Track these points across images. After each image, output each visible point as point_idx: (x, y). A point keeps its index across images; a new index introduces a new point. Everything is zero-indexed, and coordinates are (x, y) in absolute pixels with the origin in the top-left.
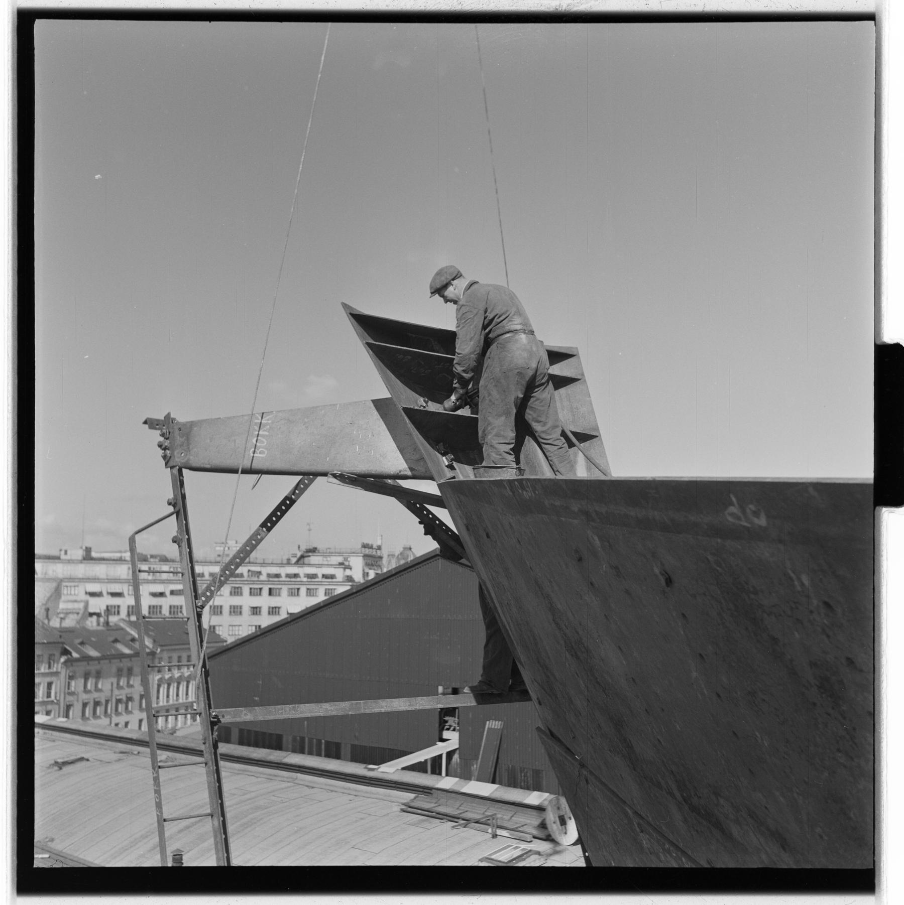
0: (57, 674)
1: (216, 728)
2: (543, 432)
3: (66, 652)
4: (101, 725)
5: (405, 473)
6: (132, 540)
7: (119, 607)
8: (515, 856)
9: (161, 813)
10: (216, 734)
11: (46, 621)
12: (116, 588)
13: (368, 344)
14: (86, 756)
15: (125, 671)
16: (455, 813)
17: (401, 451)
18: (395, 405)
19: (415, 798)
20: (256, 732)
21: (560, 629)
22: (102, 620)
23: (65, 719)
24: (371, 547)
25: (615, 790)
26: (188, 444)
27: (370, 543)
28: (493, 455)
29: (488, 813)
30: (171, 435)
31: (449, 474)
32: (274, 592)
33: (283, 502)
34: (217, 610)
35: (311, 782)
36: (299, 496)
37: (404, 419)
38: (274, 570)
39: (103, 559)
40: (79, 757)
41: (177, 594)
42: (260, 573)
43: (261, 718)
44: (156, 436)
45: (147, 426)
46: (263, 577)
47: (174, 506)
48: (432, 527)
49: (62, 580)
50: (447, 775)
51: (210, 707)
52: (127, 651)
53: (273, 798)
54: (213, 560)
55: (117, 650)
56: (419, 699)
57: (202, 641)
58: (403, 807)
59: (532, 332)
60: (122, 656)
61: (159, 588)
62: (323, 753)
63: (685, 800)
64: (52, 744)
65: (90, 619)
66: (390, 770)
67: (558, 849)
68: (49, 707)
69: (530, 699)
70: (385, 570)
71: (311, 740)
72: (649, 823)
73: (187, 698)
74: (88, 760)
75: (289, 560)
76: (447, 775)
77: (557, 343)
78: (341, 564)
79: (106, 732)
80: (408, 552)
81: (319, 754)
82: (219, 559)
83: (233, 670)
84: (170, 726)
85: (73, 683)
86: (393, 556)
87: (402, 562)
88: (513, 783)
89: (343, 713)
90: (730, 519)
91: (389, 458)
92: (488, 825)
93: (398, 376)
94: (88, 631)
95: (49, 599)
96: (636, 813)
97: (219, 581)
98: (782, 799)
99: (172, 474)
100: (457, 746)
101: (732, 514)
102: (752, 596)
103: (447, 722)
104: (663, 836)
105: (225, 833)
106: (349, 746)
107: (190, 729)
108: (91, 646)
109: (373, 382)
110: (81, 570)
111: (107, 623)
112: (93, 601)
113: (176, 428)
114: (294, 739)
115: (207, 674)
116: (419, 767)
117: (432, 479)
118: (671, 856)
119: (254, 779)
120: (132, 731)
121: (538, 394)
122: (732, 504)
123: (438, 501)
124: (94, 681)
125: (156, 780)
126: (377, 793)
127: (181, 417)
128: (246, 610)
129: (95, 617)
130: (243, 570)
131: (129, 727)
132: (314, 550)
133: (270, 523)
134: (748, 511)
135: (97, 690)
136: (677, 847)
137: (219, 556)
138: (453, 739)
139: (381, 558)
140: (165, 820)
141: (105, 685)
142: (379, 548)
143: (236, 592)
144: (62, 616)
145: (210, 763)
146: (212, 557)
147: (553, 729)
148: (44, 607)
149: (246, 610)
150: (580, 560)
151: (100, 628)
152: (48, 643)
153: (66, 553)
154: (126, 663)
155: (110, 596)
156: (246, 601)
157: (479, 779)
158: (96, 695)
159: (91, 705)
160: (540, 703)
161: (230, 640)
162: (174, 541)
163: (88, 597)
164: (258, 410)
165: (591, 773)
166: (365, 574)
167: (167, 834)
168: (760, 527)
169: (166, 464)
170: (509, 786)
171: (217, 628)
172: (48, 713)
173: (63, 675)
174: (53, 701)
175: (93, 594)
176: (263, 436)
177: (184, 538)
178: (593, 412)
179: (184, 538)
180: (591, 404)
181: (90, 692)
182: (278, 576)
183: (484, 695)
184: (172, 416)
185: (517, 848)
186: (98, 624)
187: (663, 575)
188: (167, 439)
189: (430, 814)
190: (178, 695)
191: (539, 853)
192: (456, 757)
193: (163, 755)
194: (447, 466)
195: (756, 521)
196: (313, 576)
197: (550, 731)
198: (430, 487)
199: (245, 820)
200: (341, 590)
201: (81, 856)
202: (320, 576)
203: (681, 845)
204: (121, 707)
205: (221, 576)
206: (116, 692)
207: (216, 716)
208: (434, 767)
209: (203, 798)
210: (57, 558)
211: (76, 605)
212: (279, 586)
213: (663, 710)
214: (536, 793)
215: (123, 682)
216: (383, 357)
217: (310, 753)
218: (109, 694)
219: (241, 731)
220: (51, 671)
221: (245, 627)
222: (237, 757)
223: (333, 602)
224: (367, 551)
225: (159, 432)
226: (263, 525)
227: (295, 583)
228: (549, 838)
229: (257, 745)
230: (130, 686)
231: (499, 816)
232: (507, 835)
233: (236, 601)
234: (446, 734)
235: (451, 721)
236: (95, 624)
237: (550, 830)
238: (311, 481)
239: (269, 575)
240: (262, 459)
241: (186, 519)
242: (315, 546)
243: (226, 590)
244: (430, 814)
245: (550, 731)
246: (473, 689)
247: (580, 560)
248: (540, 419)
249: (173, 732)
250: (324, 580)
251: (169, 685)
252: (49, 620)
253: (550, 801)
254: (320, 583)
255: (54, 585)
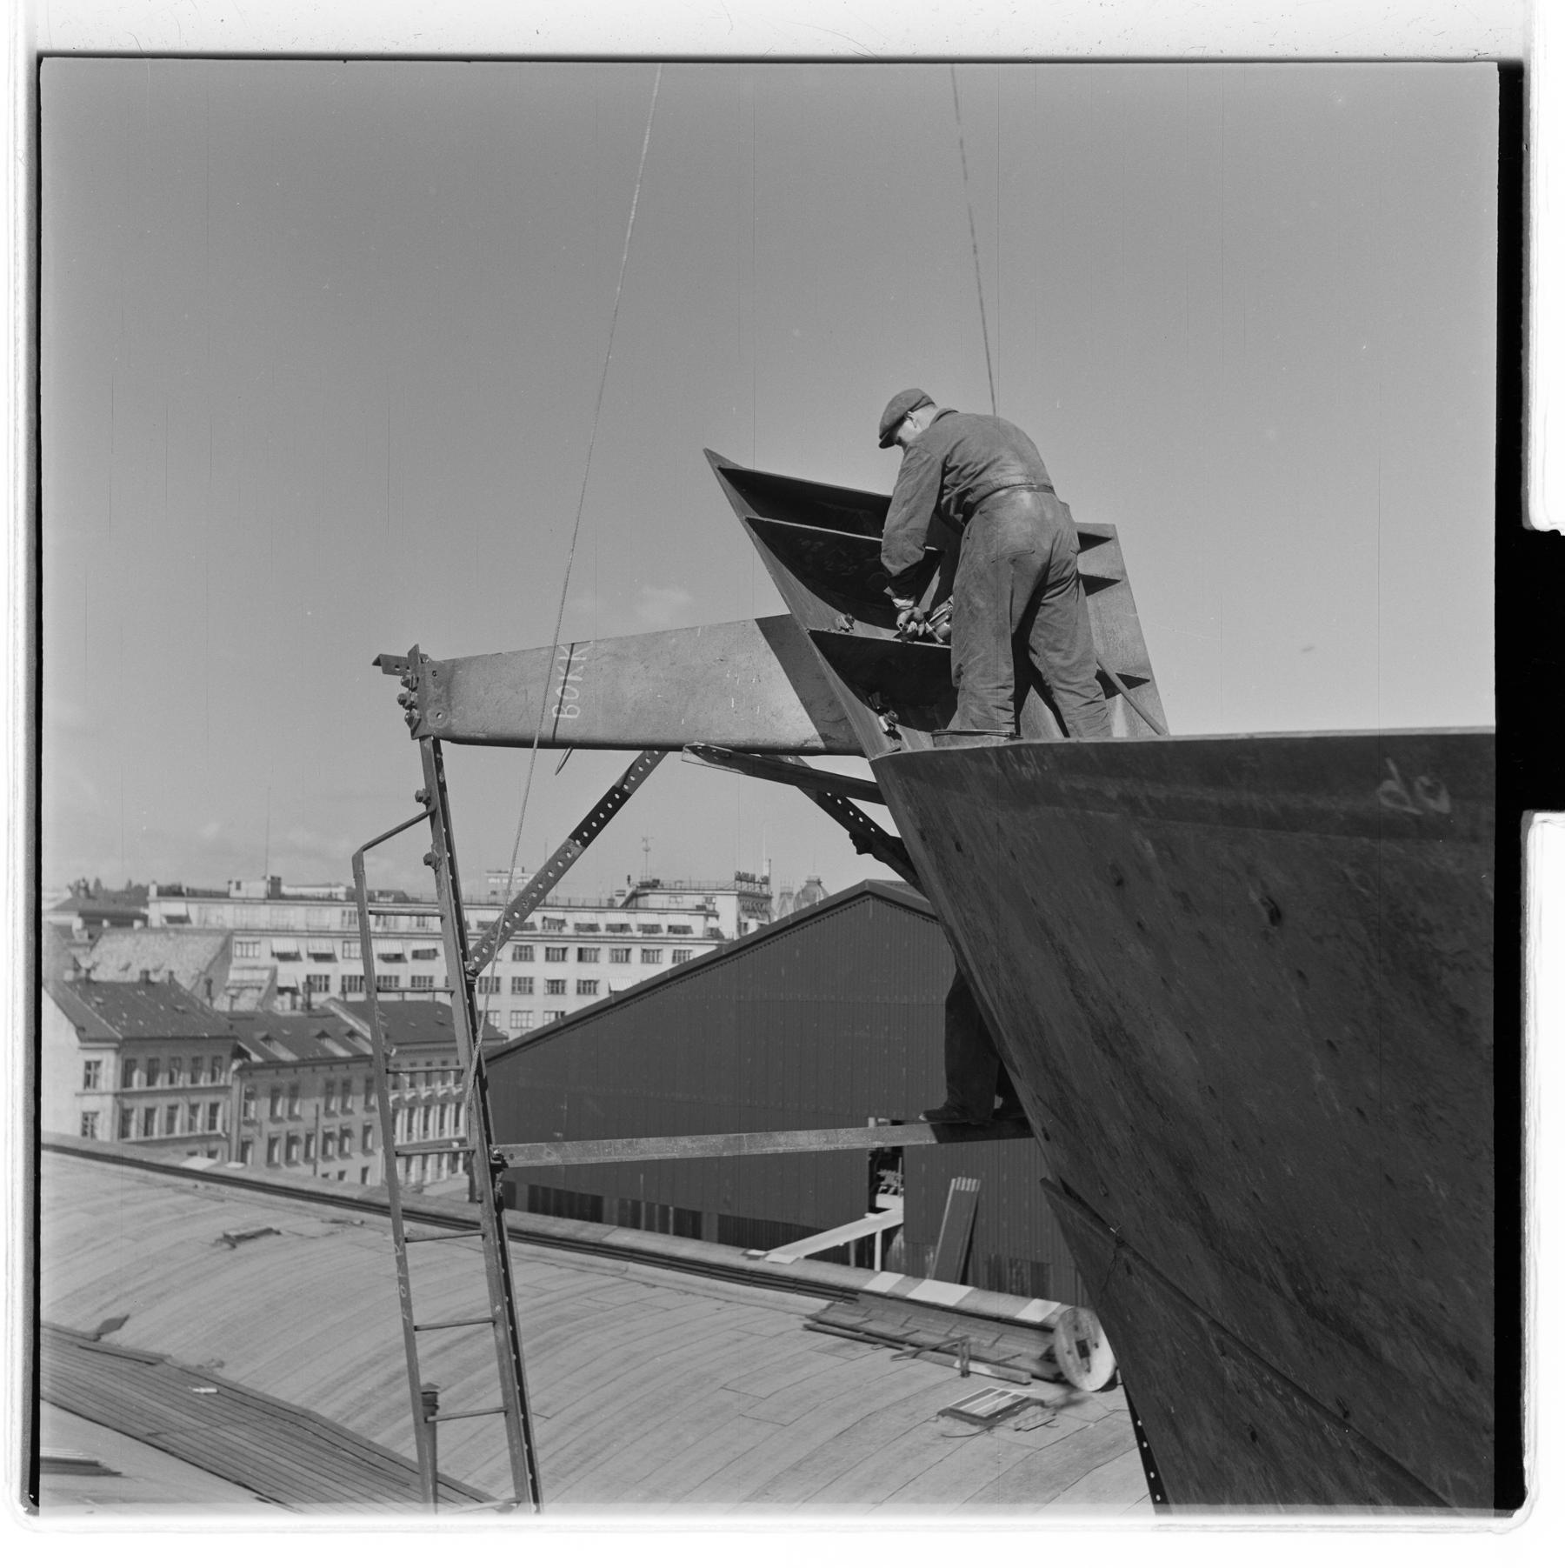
0: (225, 1089)
1: (499, 1176)
2: (1064, 669)
3: (240, 1053)
4: (300, 1175)
5: (815, 744)
6: (358, 861)
7: (327, 977)
8: (1000, 1408)
9: (410, 1315)
10: (499, 1186)
11: (207, 1002)
12: (322, 946)
13: (750, 521)
14: (275, 1227)
15: (338, 1087)
16: (898, 1333)
17: (808, 706)
18: (797, 628)
19: (829, 1307)
20: (557, 1191)
21: (1084, 1005)
22: (299, 999)
23: (240, 1165)
24: (752, 880)
25: (1177, 1283)
26: (449, 698)
27: (749, 871)
28: (974, 709)
29: (955, 1335)
30: (421, 684)
31: (889, 745)
32: (587, 955)
33: (609, 797)
34: (494, 986)
35: (655, 1277)
36: (635, 786)
37: (812, 652)
38: (587, 918)
39: (302, 897)
40: (263, 1227)
41: (423, 958)
42: (563, 922)
43: (574, 1161)
44: (394, 686)
45: (379, 669)
46: (569, 930)
47: (427, 803)
48: (867, 839)
49: (232, 933)
50: (883, 1268)
51: (489, 1141)
52: (341, 1052)
53: (588, 1303)
54: (483, 900)
55: (325, 1050)
56: (843, 1131)
57: (475, 1031)
58: (808, 1322)
59: (1050, 489)
60: (334, 1061)
61: (393, 947)
62: (671, 1229)
63: (1300, 1298)
64: (216, 1206)
65: (280, 998)
66: (785, 1258)
67: (1075, 1396)
68: (213, 1146)
69: (1030, 1135)
70: (776, 919)
71: (650, 1207)
72: (1236, 1340)
73: (441, 1134)
74: (278, 1233)
75: (611, 900)
76: (883, 1268)
77: (1086, 516)
78: (700, 908)
79: (307, 1187)
80: (816, 889)
81: (664, 1230)
82: (493, 899)
83: (527, 1082)
84: (413, 1179)
85: (252, 1105)
86: (790, 894)
87: (805, 905)
88: (997, 1284)
89: (712, 1154)
90: (1386, 802)
91: (791, 722)
92: (955, 1354)
93: (804, 577)
94: (277, 1017)
95: (211, 964)
96: (1213, 1322)
97: (496, 936)
98: (1469, 1290)
99: (422, 748)
100: (900, 1221)
101: (1389, 795)
102: (1422, 937)
103: (883, 1179)
104: (1261, 1360)
105: (516, 1351)
106: (716, 1218)
107: (444, 1184)
108: (282, 1043)
109: (762, 590)
110: (264, 916)
111: (308, 1005)
112: (285, 968)
113: (429, 671)
114: (622, 1204)
115: (483, 1084)
116: (836, 1256)
117: (862, 754)
118: (1273, 1393)
119: (555, 1271)
120: (351, 1185)
121: (1052, 599)
122: (1389, 776)
123: (871, 793)
124: (287, 1102)
125: (402, 1261)
126: (764, 1298)
127: (436, 652)
128: (540, 986)
129: (288, 995)
130: (535, 917)
131: (346, 1179)
132: (654, 885)
133: (587, 831)
134: (1418, 786)
135: (292, 1117)
136: (1285, 1380)
137: (494, 893)
138: (893, 1209)
139: (768, 898)
140: (416, 1329)
141: (307, 1108)
142: (766, 881)
143: (523, 955)
144: (233, 992)
145: (490, 1236)
146: (483, 895)
147: (1070, 1184)
148: (203, 978)
149: (540, 986)
150: (1120, 883)
151: (297, 1013)
152: (210, 1038)
153: (238, 886)
154: (339, 1074)
155: (312, 961)
156: (540, 970)
157: (939, 1277)
158: (290, 1126)
159: (283, 1142)
160: (1047, 1138)
161: (513, 1035)
162: (427, 863)
163: (276, 961)
164: (566, 639)
165: (1136, 1254)
166: (742, 926)
167: (421, 1353)
168: (1439, 814)
169: (413, 733)
170: (991, 1289)
171: (491, 1016)
172: (211, 1155)
173: (235, 1092)
174: (218, 1136)
175: (284, 957)
176: (574, 683)
177: (443, 859)
178: (1139, 638)
179: (443, 859)
180: (1137, 623)
181: (280, 1120)
182: (593, 927)
183: (955, 1125)
184: (422, 651)
185: (1003, 1394)
186: (294, 1007)
187: (1264, 904)
188: (414, 690)
189: (854, 1334)
190: (426, 1128)
191: (1041, 1403)
192: (899, 1239)
193: (408, 1226)
194: (887, 733)
195: (1431, 803)
196: (655, 929)
197: (1064, 1184)
198: (858, 769)
199: (541, 1338)
200: (698, 952)
201: (270, 1393)
202: (665, 928)
203: (1292, 1376)
204: (332, 1147)
205: (506, 920)
206: (324, 1121)
207: (499, 1157)
208: (862, 1254)
209: (478, 1297)
210: (222, 896)
211: (257, 975)
212: (596, 946)
213: (1262, 1141)
214: (1037, 1302)
215: (335, 1104)
216: (775, 542)
217: (650, 1228)
218: (312, 1125)
219: (533, 1189)
220: (216, 1084)
221: (538, 1013)
222: (527, 1233)
223: (686, 972)
224: (745, 886)
225: (400, 678)
226: (576, 835)
227: (623, 940)
228: (1059, 1379)
229: (559, 1213)
230: (345, 1111)
231: (973, 1339)
232: (987, 1372)
233: (523, 969)
234: (882, 1200)
235: (890, 1177)
236: (288, 1006)
237: (1061, 1365)
238: (657, 761)
239: (578, 926)
240: (572, 723)
241: (447, 825)
242: (656, 877)
243: (506, 952)
244: (854, 1334)
245: (1064, 1184)
246: (930, 1116)
247: (1120, 883)
248: (1059, 646)
249: (419, 1188)
250: (671, 935)
251: (411, 1111)
252: (212, 999)
253: (1062, 1317)
254: (665, 941)
255: (220, 940)
